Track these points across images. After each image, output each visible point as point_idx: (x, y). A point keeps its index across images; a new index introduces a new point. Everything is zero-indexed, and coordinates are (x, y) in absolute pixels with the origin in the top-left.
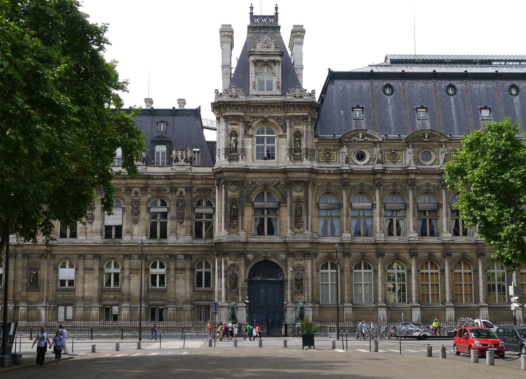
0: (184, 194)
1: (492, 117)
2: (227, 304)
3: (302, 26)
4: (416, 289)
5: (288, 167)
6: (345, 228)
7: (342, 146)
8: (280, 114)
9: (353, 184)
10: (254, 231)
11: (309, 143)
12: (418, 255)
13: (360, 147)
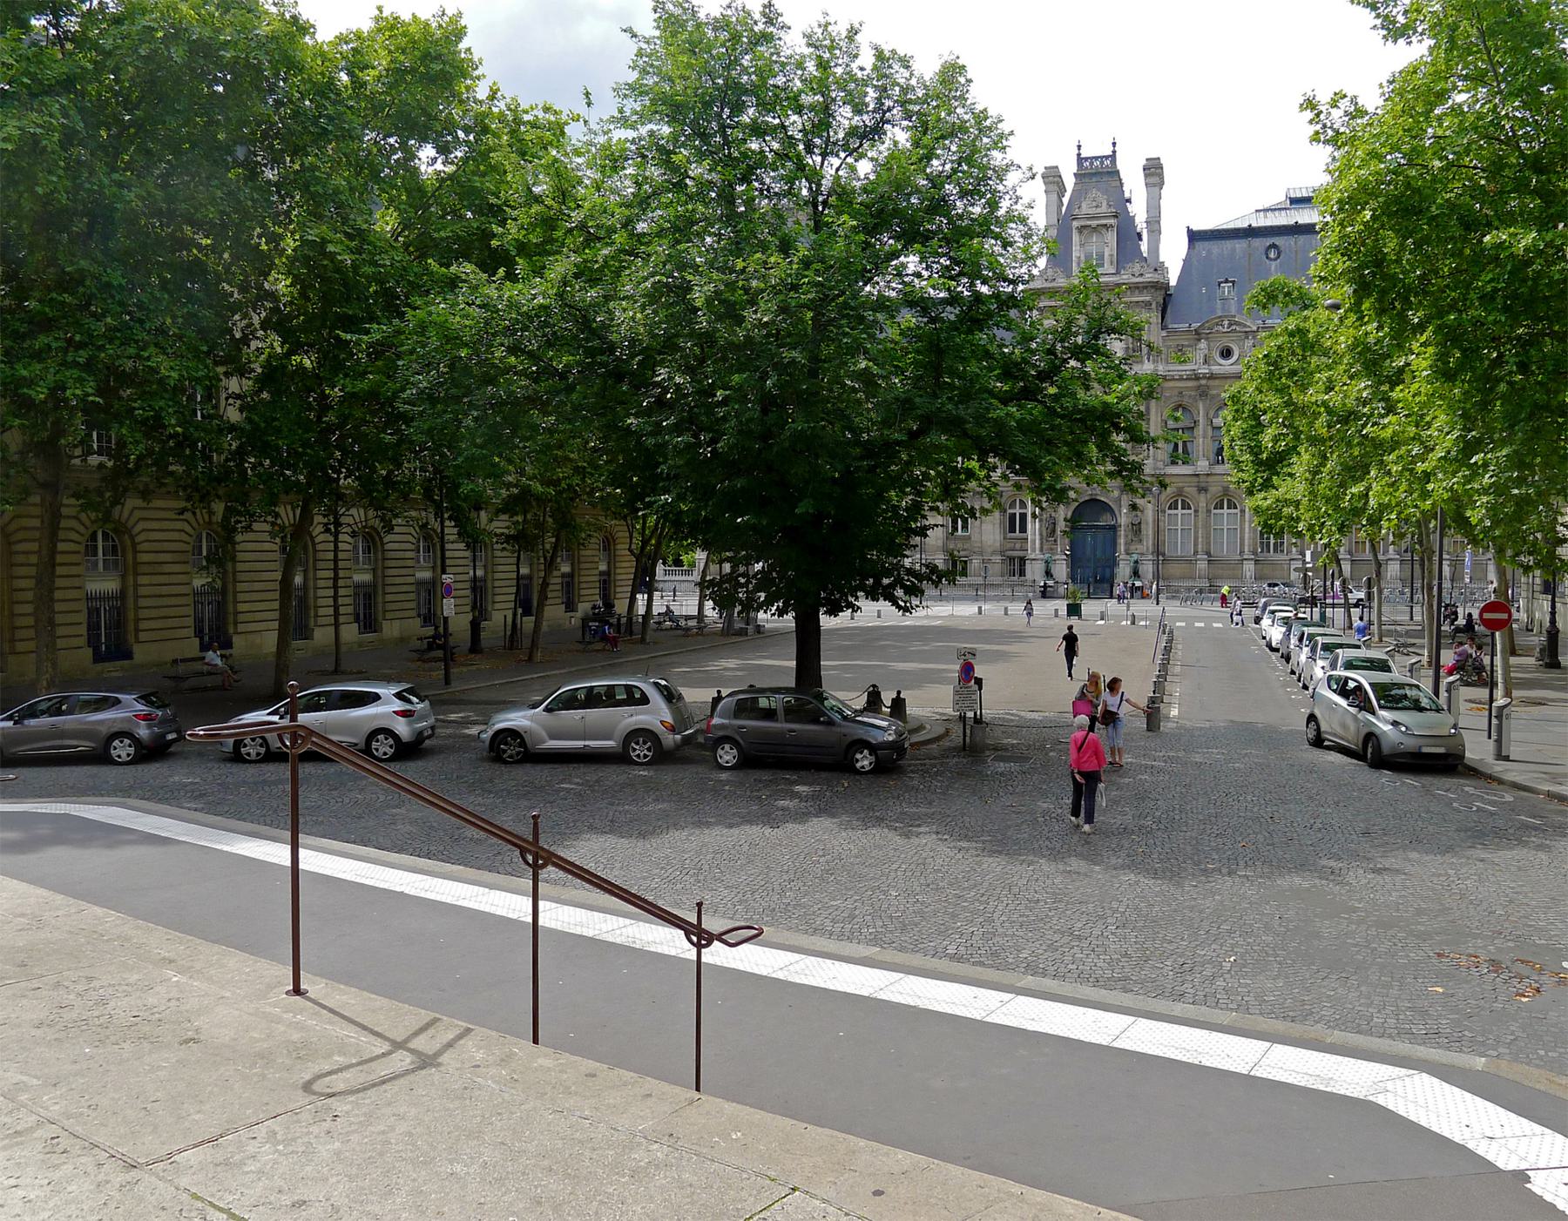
7: (1199, 340)
13: (1225, 340)
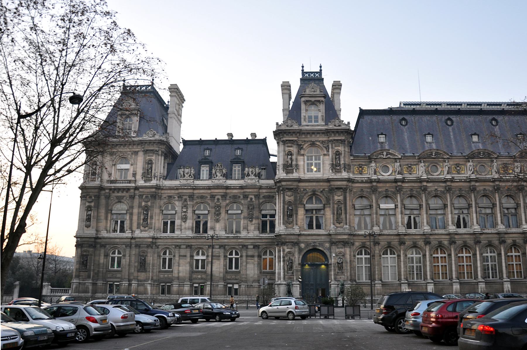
0: (254, 200)
1: (480, 141)
2: (285, 282)
3: (340, 81)
4: (430, 270)
5: (330, 177)
6: (375, 223)
7: (371, 162)
8: (324, 138)
9: (380, 190)
10: (306, 226)
11: (346, 160)
12: (431, 243)
